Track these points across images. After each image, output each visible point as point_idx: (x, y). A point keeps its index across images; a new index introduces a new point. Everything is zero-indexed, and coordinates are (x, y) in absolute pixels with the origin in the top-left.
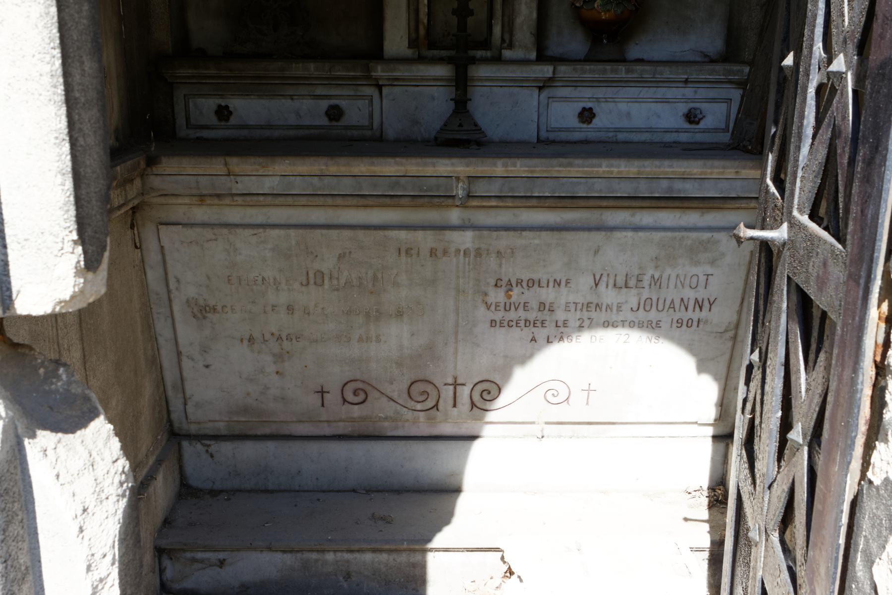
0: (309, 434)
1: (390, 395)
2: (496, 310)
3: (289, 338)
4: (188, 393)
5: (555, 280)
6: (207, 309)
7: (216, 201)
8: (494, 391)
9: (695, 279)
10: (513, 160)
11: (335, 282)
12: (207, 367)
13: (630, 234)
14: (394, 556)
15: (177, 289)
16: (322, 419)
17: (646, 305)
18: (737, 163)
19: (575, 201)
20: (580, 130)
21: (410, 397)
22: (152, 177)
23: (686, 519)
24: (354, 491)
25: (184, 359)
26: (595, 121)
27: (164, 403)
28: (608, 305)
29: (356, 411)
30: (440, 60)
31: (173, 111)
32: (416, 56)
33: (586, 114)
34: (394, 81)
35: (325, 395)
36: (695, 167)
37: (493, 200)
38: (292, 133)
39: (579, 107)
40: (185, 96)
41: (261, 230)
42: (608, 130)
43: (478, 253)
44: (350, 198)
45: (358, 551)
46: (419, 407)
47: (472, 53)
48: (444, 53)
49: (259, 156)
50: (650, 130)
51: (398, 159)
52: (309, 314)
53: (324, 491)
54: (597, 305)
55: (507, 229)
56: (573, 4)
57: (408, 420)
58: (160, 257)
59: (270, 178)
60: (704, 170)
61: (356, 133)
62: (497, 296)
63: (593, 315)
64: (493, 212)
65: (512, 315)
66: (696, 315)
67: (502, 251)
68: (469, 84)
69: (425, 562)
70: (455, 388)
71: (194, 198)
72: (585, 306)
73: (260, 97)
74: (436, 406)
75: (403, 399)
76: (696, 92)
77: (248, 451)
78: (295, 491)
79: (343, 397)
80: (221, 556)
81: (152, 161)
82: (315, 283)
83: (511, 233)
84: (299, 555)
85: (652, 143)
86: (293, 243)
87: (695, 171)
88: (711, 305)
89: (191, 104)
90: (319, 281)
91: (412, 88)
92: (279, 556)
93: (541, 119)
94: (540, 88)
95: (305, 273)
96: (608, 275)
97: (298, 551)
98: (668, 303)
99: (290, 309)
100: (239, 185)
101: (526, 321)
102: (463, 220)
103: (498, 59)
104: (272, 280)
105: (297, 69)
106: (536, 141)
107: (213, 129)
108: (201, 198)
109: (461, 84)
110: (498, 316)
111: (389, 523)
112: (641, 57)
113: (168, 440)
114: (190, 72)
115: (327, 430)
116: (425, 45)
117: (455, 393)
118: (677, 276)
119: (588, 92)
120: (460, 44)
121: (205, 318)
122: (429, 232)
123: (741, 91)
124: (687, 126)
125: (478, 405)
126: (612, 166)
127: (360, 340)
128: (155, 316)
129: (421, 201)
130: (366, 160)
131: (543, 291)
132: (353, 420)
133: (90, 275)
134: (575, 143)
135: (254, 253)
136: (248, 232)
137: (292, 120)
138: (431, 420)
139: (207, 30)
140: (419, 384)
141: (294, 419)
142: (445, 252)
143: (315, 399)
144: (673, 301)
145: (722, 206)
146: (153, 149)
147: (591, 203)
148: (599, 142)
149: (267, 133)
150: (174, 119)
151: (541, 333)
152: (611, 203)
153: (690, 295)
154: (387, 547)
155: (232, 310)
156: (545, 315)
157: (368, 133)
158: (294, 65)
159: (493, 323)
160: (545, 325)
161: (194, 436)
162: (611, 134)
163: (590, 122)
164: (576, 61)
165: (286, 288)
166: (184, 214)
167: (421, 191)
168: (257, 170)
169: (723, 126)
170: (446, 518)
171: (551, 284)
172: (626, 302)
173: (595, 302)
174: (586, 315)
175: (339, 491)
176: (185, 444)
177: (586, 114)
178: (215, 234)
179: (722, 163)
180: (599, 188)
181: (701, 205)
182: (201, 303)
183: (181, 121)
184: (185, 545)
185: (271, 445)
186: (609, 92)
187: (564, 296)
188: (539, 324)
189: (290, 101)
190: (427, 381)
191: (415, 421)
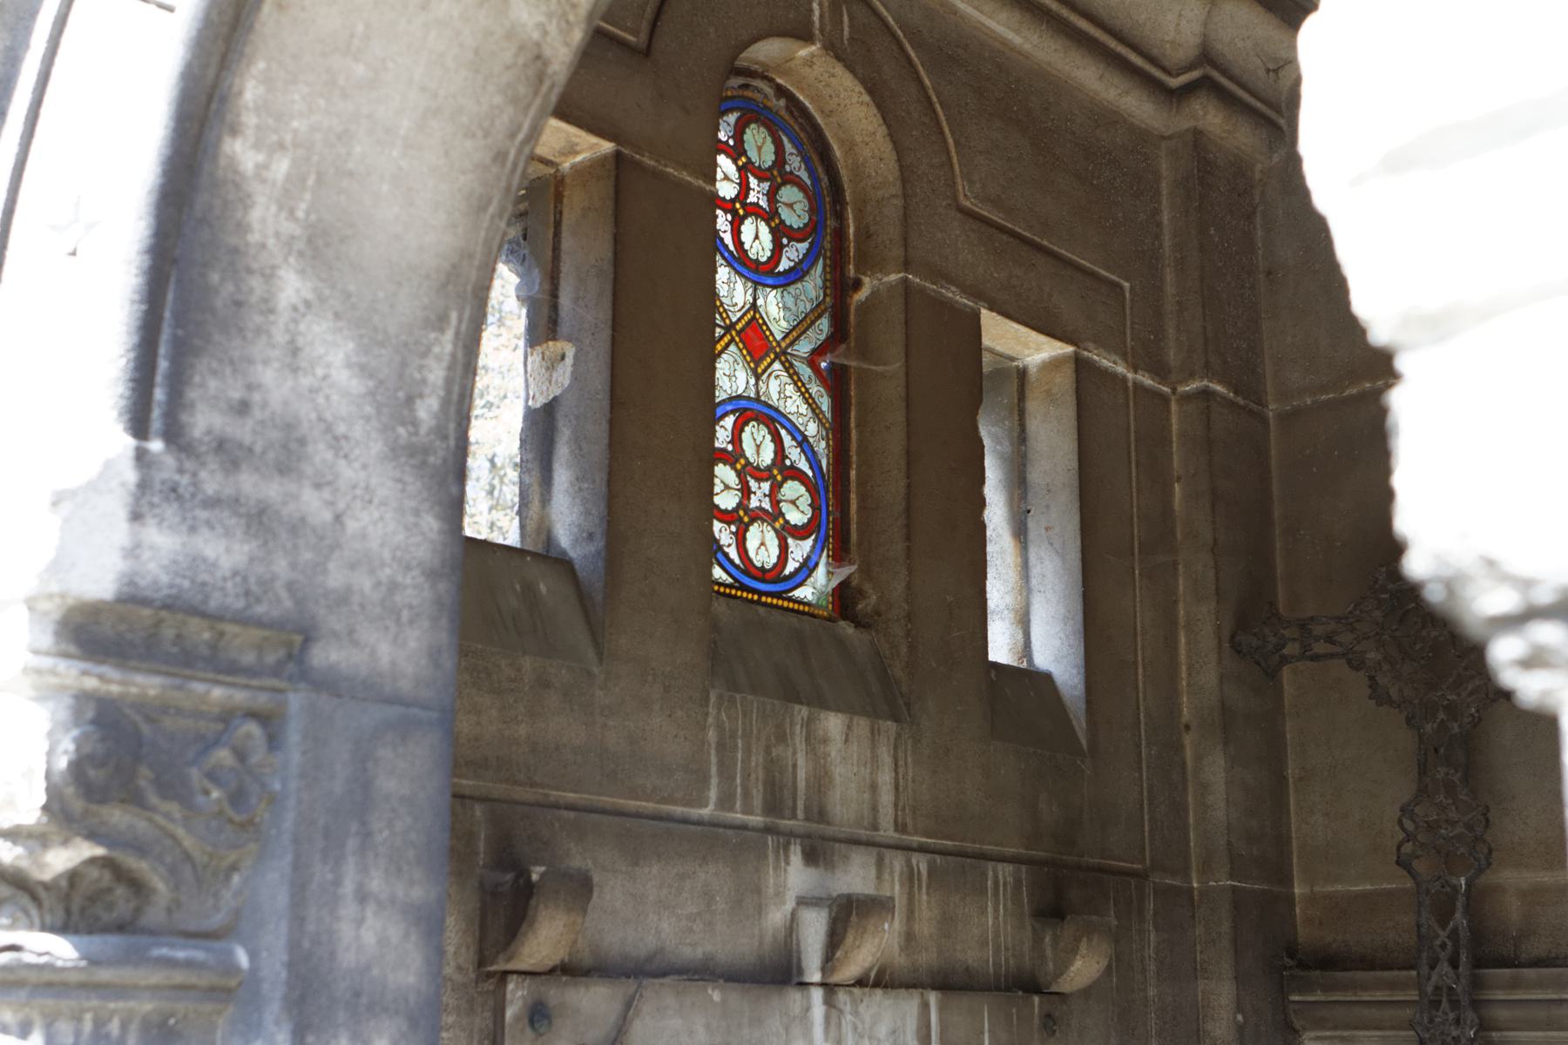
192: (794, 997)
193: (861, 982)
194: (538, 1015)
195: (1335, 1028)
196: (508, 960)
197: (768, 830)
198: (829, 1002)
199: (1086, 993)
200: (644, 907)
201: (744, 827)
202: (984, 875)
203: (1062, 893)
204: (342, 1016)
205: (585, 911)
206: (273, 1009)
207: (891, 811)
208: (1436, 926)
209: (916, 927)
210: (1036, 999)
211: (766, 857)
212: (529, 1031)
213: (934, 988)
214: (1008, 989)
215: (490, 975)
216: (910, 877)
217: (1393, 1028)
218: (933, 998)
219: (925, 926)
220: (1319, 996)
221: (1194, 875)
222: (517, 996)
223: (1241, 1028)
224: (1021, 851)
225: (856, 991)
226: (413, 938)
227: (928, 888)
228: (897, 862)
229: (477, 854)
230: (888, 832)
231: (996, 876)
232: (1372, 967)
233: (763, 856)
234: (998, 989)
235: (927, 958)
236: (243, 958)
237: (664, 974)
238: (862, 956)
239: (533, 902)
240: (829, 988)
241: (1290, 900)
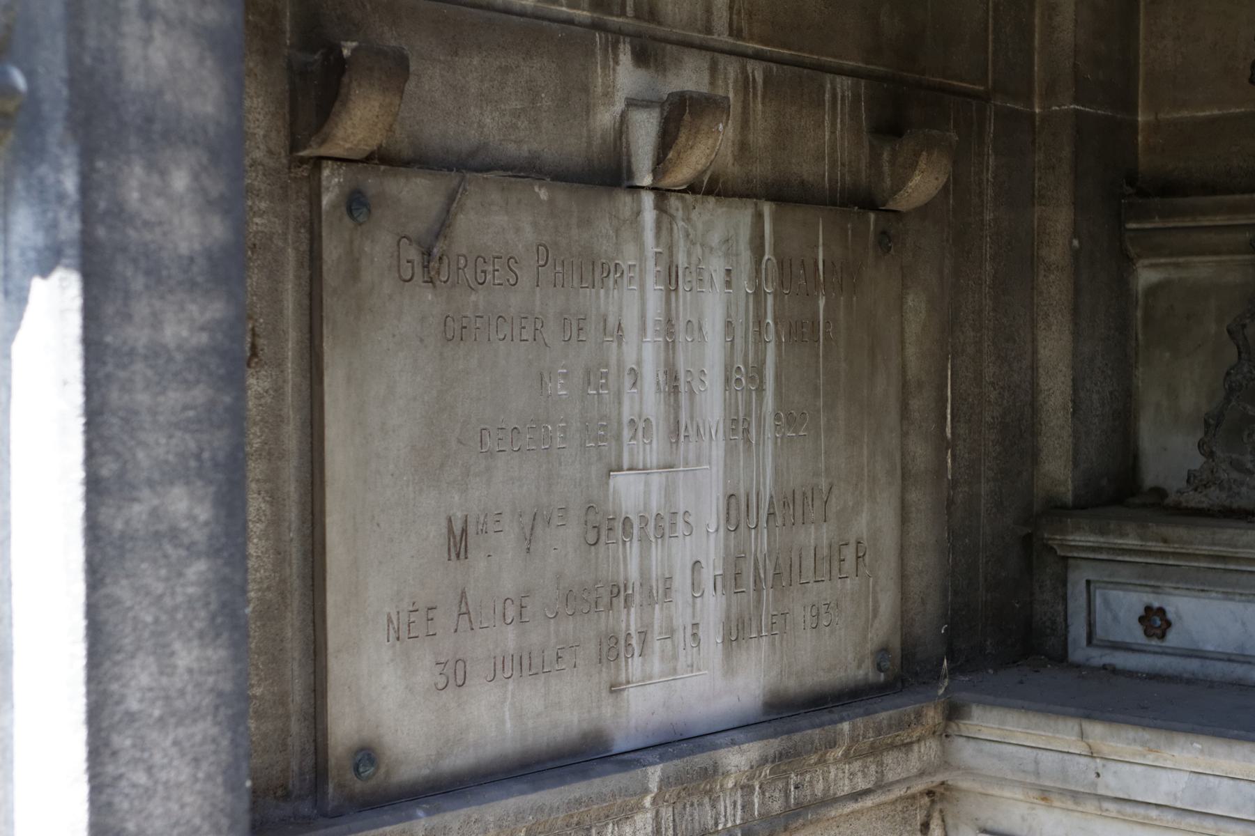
40: (1088, 582)
59: (1171, 775)
73: (1227, 596)
81: (954, 712)
89: (1098, 601)
107: (1133, 650)
114: (1092, 539)
150: (1067, 626)
166: (1023, 819)
183: (1078, 630)
192: (625, 201)
193: (692, 188)
194: (356, 203)
195: (1171, 255)
196: (323, 142)
197: (596, 26)
198: (660, 207)
199: (924, 211)
200: (466, 98)
201: (570, 22)
202: (822, 87)
203: (896, 113)
204: (134, 142)
205: (401, 92)
206: (57, 131)
207: (725, 14)
209: (751, 137)
210: (872, 216)
211: (593, 54)
212: (347, 219)
213: (769, 198)
214: (843, 205)
215: (303, 161)
216: (746, 84)
217: (1231, 252)
218: (767, 208)
219: (760, 137)
220: (1157, 223)
221: (1037, 101)
222: (333, 184)
223: (1076, 254)
224: (860, 64)
225: (688, 197)
226: (209, 63)
227: (764, 97)
228: (731, 68)
229: (284, 33)
230: (722, 37)
231: (834, 89)
233: (589, 53)
234: (834, 204)
235: (761, 170)
236: (20, 80)
237: (488, 169)
238: (694, 160)
239: (345, 79)
240: (661, 193)
241: (1134, 126)
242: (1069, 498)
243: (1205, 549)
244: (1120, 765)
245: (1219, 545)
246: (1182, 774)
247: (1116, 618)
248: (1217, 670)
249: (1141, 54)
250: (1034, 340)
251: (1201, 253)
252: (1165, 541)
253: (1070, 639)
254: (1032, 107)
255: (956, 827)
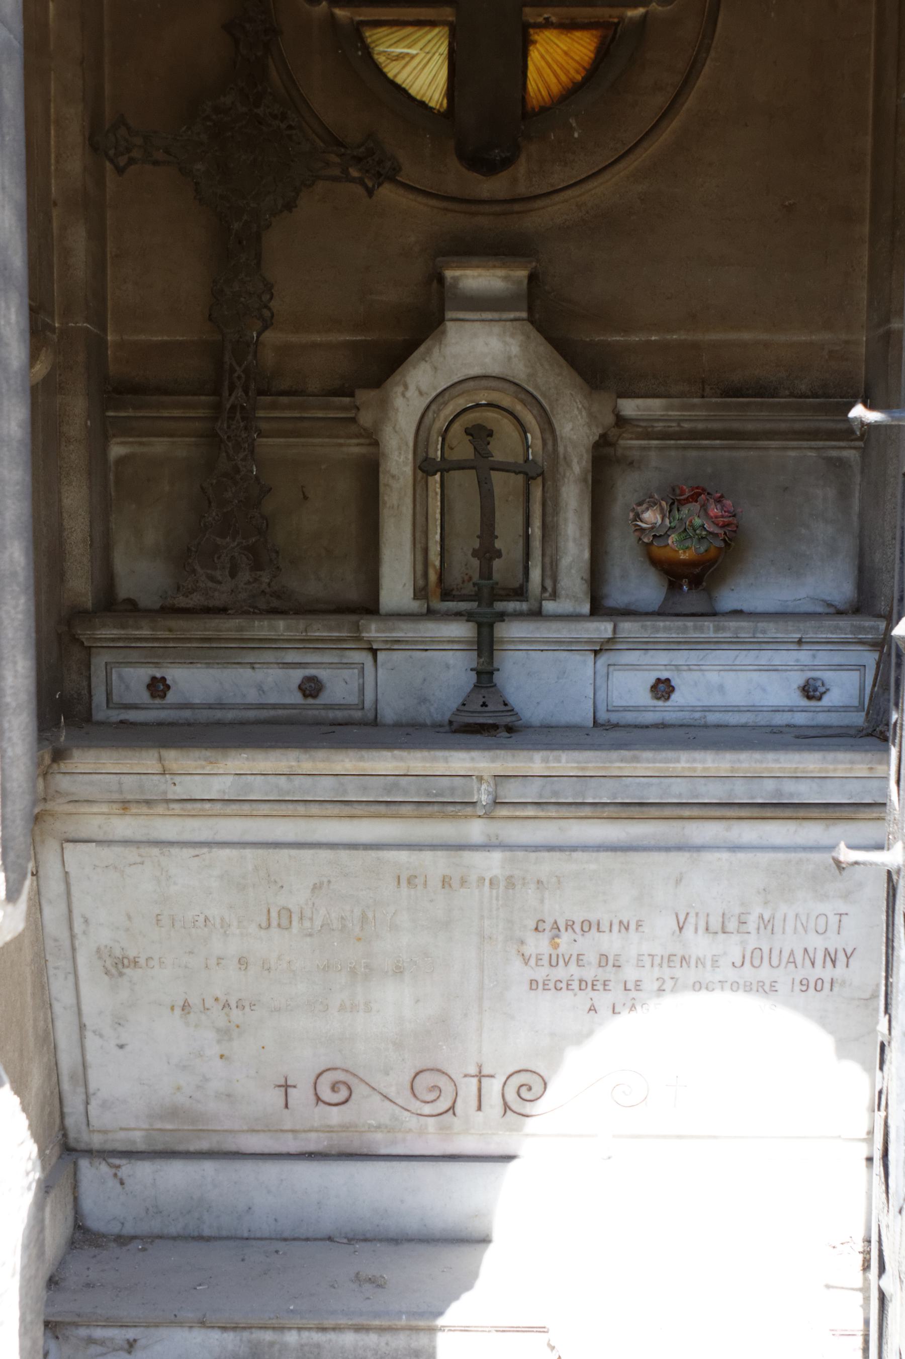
0: (267, 1151)
1: (384, 1091)
2: (537, 965)
3: (240, 1006)
4: (92, 1087)
5: (621, 922)
6: (126, 961)
7: (145, 809)
8: (537, 1087)
9: (822, 921)
10: (556, 753)
11: (307, 924)
12: (121, 1047)
13: (725, 855)
14: (387, 1337)
15: (84, 933)
16: (285, 1128)
17: (754, 958)
18: (869, 755)
19: (645, 809)
20: (654, 709)
21: (415, 1095)
22: (59, 777)
23: (828, 1287)
24: (330, 1239)
25: (89, 1034)
26: (674, 696)
27: (57, 1102)
28: (698, 959)
29: (335, 1116)
30: (458, 615)
31: (89, 686)
32: (425, 610)
33: (661, 686)
34: (394, 645)
35: (290, 1090)
36: (810, 762)
37: (529, 807)
38: (251, 714)
39: (651, 678)
41: (205, 850)
42: (693, 709)
43: (510, 882)
44: (329, 806)
45: (334, 1329)
46: (427, 1109)
47: (500, 606)
48: (463, 606)
49: (206, 748)
50: (752, 709)
51: (396, 752)
52: (269, 969)
53: (285, 1240)
54: (683, 958)
55: (551, 848)
56: (640, 539)
57: (410, 1130)
58: (62, 887)
59: (220, 778)
60: (824, 766)
61: (340, 715)
62: (538, 945)
63: (678, 972)
64: (530, 824)
65: (561, 973)
66: (827, 973)
67: (544, 880)
68: (495, 647)
69: (434, 1348)
70: (480, 1082)
71: (115, 806)
72: (666, 960)
73: (209, 665)
74: (452, 1107)
75: (405, 1098)
76: (814, 656)
77: (176, 1176)
78: (242, 1239)
79: (316, 1094)
80: (131, 1334)
82: (279, 925)
83: (557, 855)
84: (246, 1334)
85: (755, 727)
86: (250, 867)
87: (812, 767)
88: (848, 958)
89: (114, 677)
90: (284, 922)
91: (419, 653)
92: (215, 1336)
93: (598, 694)
94: (596, 652)
95: (265, 911)
96: (697, 914)
97: (244, 1328)
98: (785, 955)
99: (243, 962)
100: (178, 788)
101: (581, 981)
102: (488, 836)
103: (537, 614)
104: (218, 921)
105: (262, 628)
106: (592, 725)
108: (125, 805)
109: (486, 646)
110: (541, 974)
111: (379, 1286)
112: (739, 608)
113: (60, 1157)
115: (291, 1145)
116: (439, 593)
117: (480, 1090)
118: (797, 915)
119: (662, 658)
120: (484, 594)
121: (121, 974)
122: (439, 853)
123: (876, 655)
124: (804, 702)
125: (514, 1107)
126: (694, 761)
127: (342, 1008)
128: (51, 972)
129: (429, 809)
130: (352, 753)
131: (605, 938)
132: (330, 1130)
133: (10, 908)
134: (647, 727)
135: (194, 881)
136: (188, 852)
137: (252, 697)
138: (445, 1130)
139: (141, 573)
140: (426, 1075)
141: (245, 1128)
142: (463, 882)
143: (277, 1097)
144: (792, 953)
145: (853, 816)
146: (62, 739)
147: (667, 812)
148: (681, 726)
149: (219, 714)
151: (603, 1000)
152: (696, 812)
153: (817, 943)
154: (377, 1323)
155: (161, 963)
156: (608, 973)
157: (357, 715)
158: (256, 623)
159: (533, 984)
160: (603, 985)
161: (98, 1152)
162: (697, 715)
163: (668, 698)
164: (647, 614)
165: (237, 932)
166: (100, 827)
167: (428, 795)
168: (203, 767)
169: (856, 703)
170: (466, 1282)
171: (616, 928)
172: (725, 953)
173: (680, 953)
174: (667, 972)
175: (307, 1239)
176: (84, 1163)
177: (661, 686)
178: (140, 855)
179: (849, 756)
180: (679, 791)
181: (824, 815)
182: (118, 953)
183: (99, 697)
184: (79, 1315)
185: (208, 1167)
186: (693, 657)
187: (630, 946)
188: (599, 986)
189: (249, 671)
190: (439, 1071)
191: (422, 1132)
208: (234, 364)
217: (183, 436)
221: (56, 318)
232: (166, 392)
241: (106, 341)
242: (89, 605)
243: (199, 634)
244: (183, 776)
245: (209, 630)
246: (228, 776)
247: (127, 687)
248: (204, 715)
249: (109, 293)
250: (60, 492)
251: (162, 435)
252: (170, 630)
253: (94, 705)
254: (54, 322)
255: (43, 842)
